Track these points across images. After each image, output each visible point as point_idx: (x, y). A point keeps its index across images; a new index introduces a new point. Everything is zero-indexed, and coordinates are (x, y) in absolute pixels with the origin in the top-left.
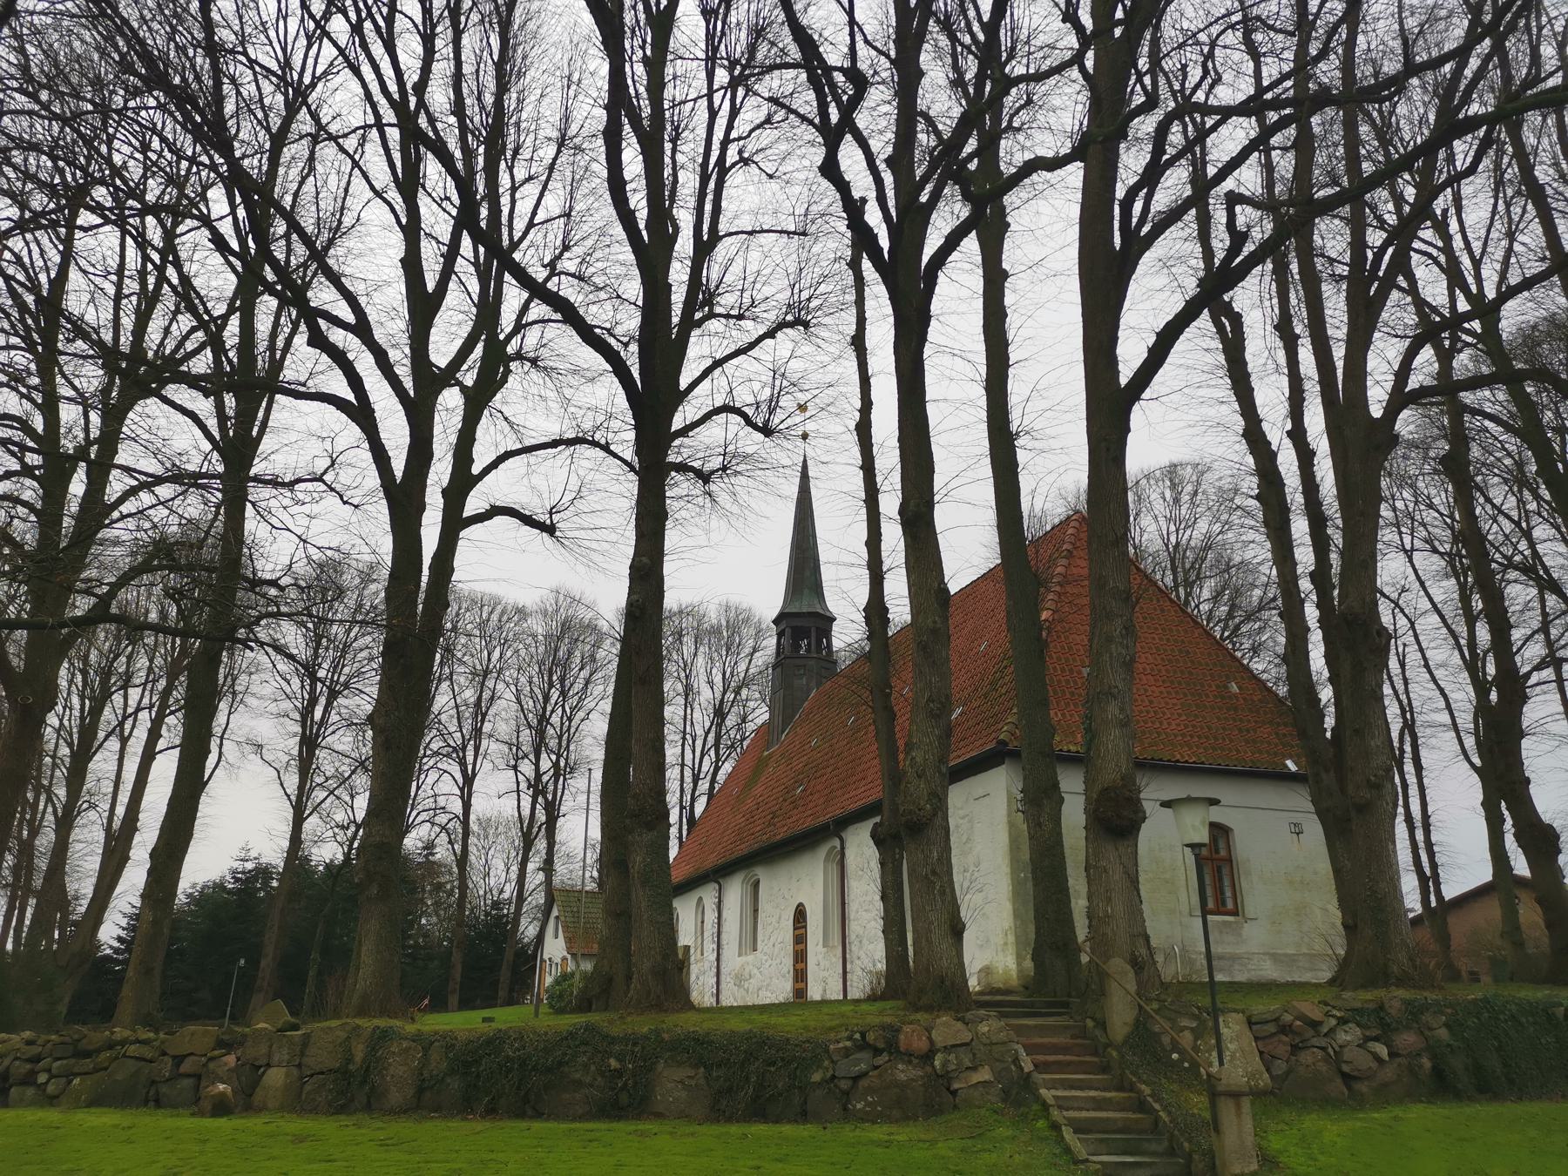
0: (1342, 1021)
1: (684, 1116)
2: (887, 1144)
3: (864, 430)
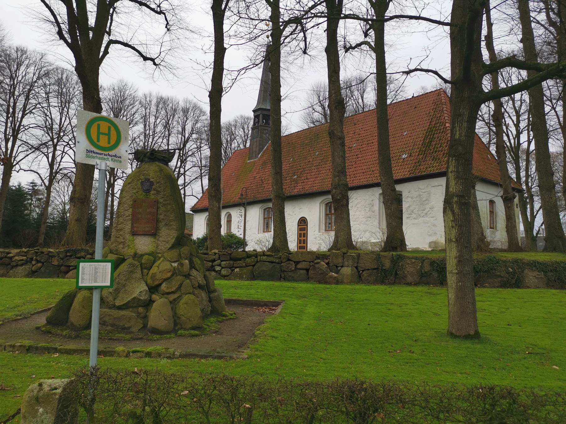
1: (537, 287)
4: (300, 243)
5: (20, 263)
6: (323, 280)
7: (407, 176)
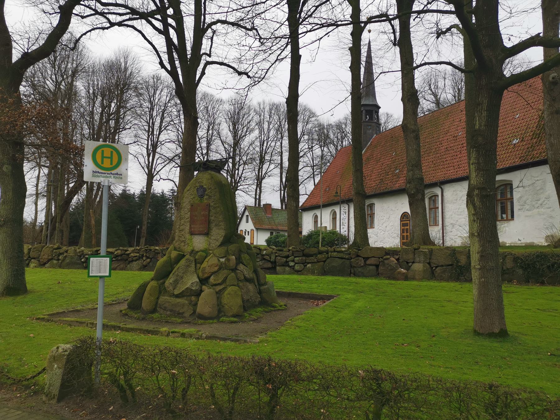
4: (403, 239)
5: (134, 259)
6: (392, 276)
7: (517, 164)
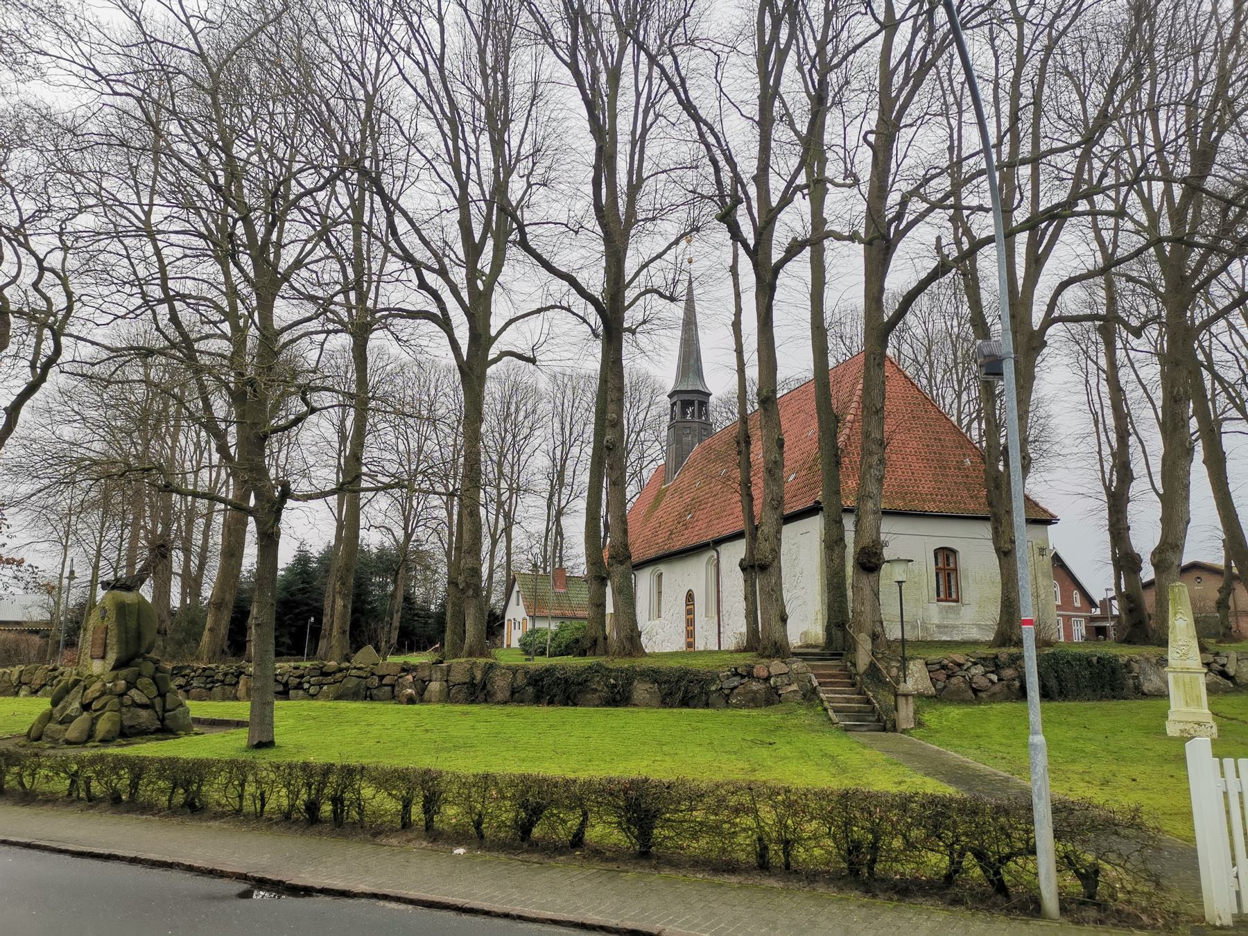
0: (975, 664)
1: (647, 705)
2: (748, 716)
3: (737, 325)
